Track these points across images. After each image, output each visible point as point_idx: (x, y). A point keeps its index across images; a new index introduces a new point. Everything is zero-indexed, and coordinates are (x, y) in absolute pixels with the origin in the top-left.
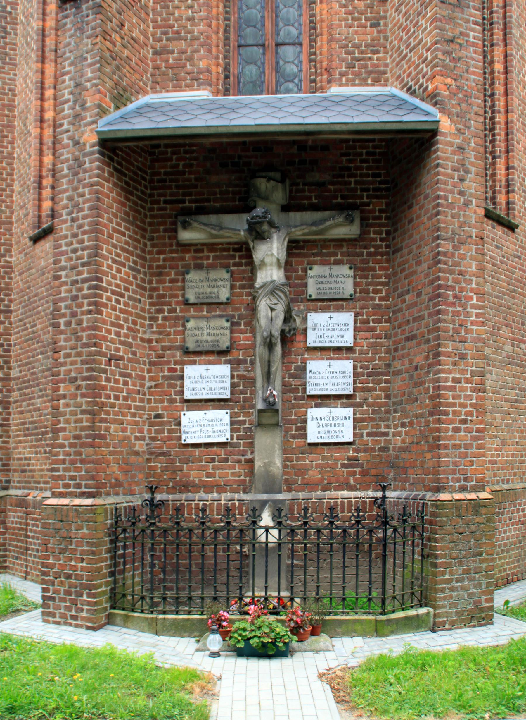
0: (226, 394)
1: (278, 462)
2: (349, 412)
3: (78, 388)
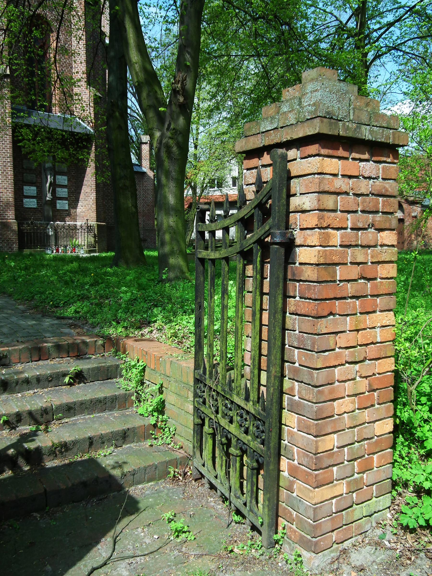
0: (35, 195)
1: (51, 213)
2: (67, 202)
3: (8, 191)
